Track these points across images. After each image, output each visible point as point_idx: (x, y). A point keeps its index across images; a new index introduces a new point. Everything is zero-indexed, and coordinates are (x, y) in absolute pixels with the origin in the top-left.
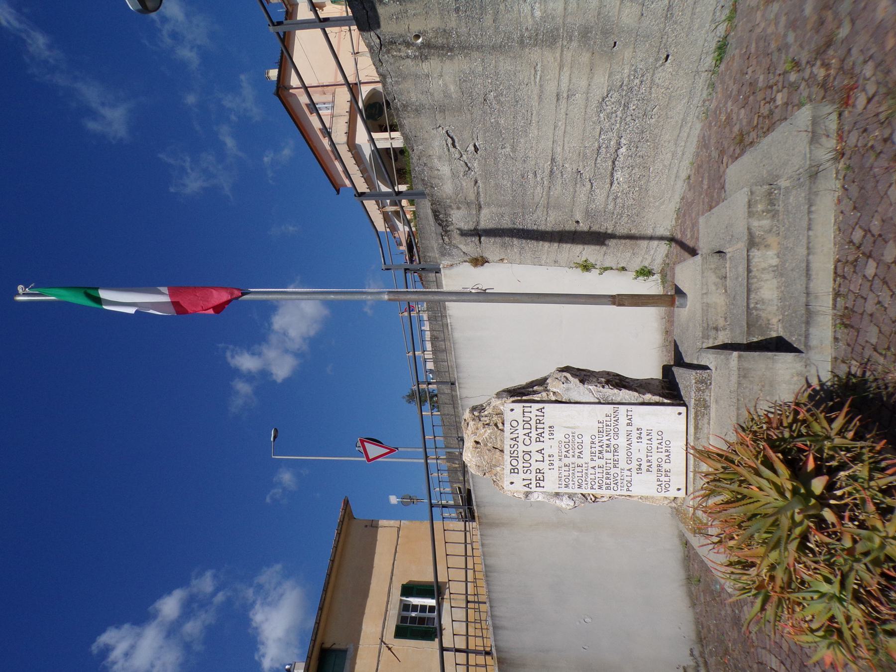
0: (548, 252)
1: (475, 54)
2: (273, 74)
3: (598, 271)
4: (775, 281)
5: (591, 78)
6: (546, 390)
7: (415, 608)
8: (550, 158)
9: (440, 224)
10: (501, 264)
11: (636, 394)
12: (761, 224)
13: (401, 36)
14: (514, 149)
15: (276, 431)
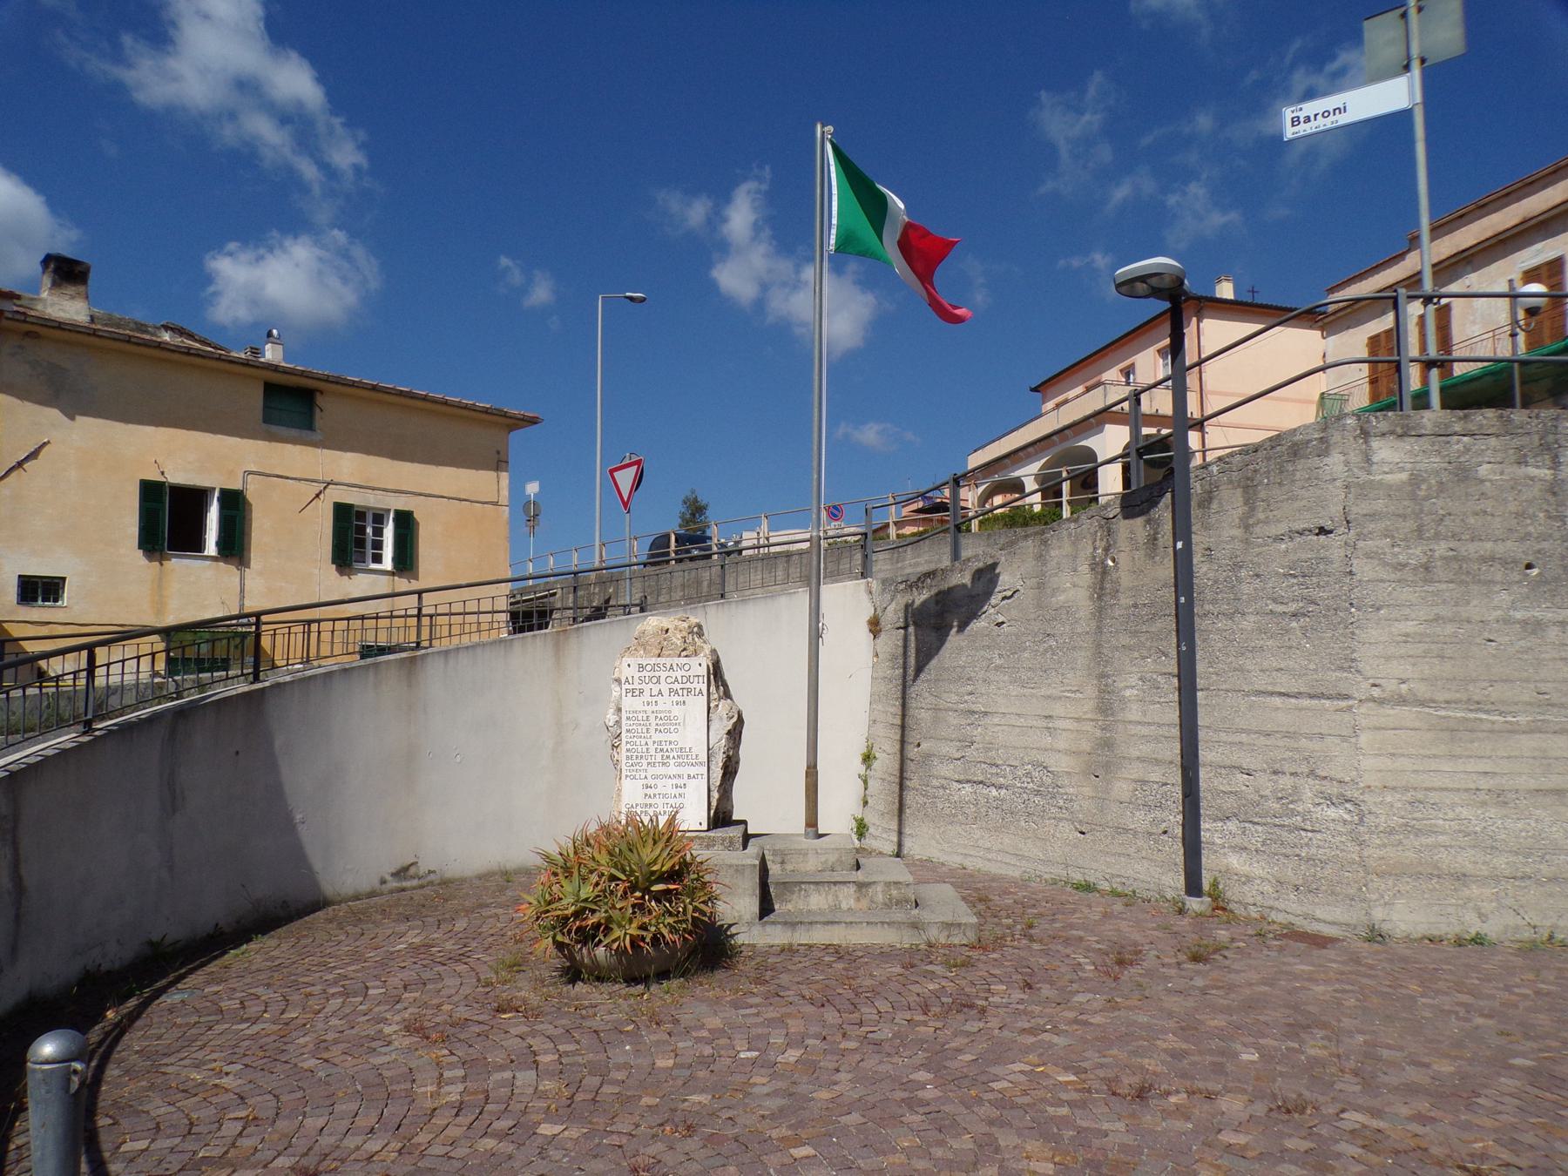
0: (886, 712)
1: (1093, 624)
2: (1226, 291)
3: (863, 772)
4: (826, 907)
5: (1068, 752)
6: (720, 698)
7: (378, 532)
8: (988, 710)
9: (920, 578)
10: (871, 655)
11: (718, 784)
12: (878, 893)
13: (1115, 543)
14: (997, 668)
15: (643, 300)
